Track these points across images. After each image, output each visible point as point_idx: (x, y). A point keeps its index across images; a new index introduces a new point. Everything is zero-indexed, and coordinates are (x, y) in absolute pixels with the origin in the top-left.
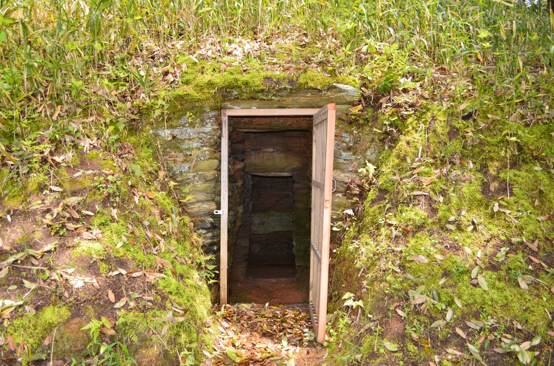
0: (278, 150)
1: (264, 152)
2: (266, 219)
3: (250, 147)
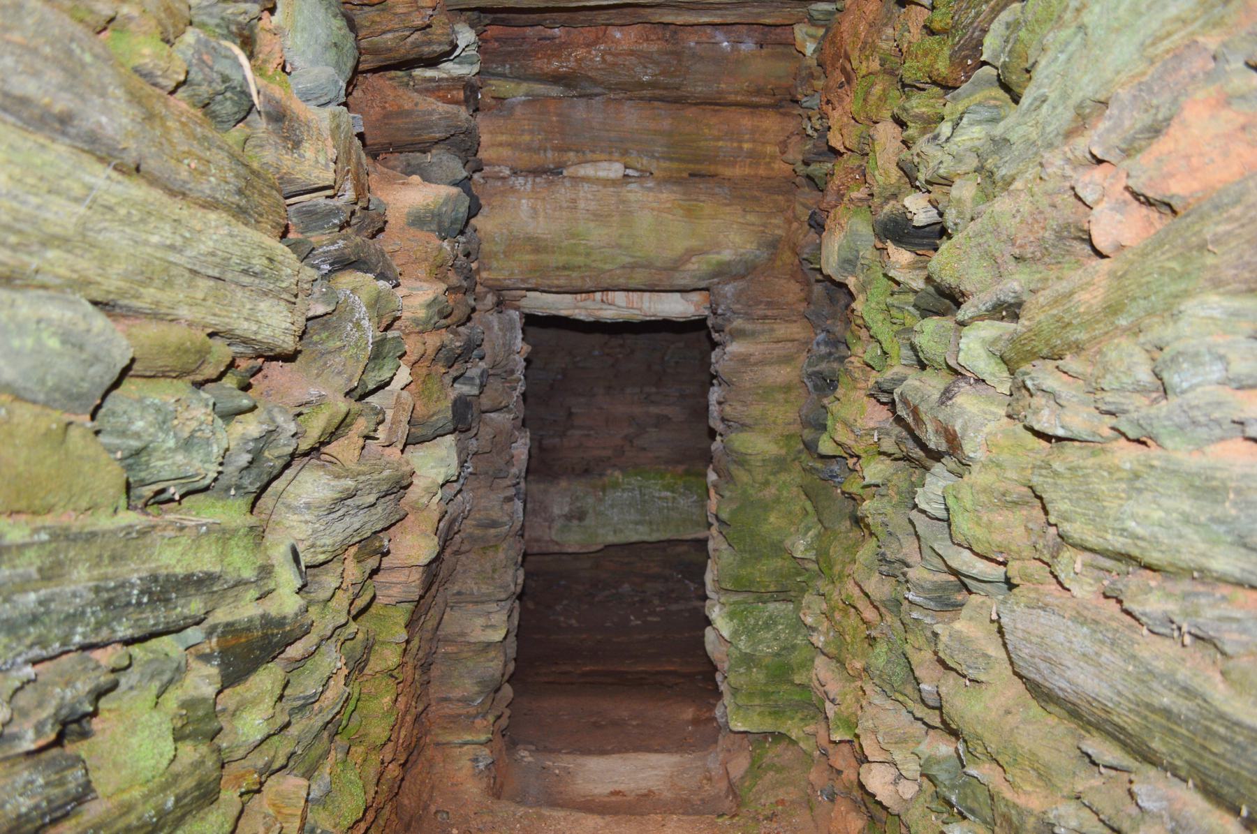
0: (645, 174)
1: (576, 180)
2: (591, 500)
3: (506, 152)
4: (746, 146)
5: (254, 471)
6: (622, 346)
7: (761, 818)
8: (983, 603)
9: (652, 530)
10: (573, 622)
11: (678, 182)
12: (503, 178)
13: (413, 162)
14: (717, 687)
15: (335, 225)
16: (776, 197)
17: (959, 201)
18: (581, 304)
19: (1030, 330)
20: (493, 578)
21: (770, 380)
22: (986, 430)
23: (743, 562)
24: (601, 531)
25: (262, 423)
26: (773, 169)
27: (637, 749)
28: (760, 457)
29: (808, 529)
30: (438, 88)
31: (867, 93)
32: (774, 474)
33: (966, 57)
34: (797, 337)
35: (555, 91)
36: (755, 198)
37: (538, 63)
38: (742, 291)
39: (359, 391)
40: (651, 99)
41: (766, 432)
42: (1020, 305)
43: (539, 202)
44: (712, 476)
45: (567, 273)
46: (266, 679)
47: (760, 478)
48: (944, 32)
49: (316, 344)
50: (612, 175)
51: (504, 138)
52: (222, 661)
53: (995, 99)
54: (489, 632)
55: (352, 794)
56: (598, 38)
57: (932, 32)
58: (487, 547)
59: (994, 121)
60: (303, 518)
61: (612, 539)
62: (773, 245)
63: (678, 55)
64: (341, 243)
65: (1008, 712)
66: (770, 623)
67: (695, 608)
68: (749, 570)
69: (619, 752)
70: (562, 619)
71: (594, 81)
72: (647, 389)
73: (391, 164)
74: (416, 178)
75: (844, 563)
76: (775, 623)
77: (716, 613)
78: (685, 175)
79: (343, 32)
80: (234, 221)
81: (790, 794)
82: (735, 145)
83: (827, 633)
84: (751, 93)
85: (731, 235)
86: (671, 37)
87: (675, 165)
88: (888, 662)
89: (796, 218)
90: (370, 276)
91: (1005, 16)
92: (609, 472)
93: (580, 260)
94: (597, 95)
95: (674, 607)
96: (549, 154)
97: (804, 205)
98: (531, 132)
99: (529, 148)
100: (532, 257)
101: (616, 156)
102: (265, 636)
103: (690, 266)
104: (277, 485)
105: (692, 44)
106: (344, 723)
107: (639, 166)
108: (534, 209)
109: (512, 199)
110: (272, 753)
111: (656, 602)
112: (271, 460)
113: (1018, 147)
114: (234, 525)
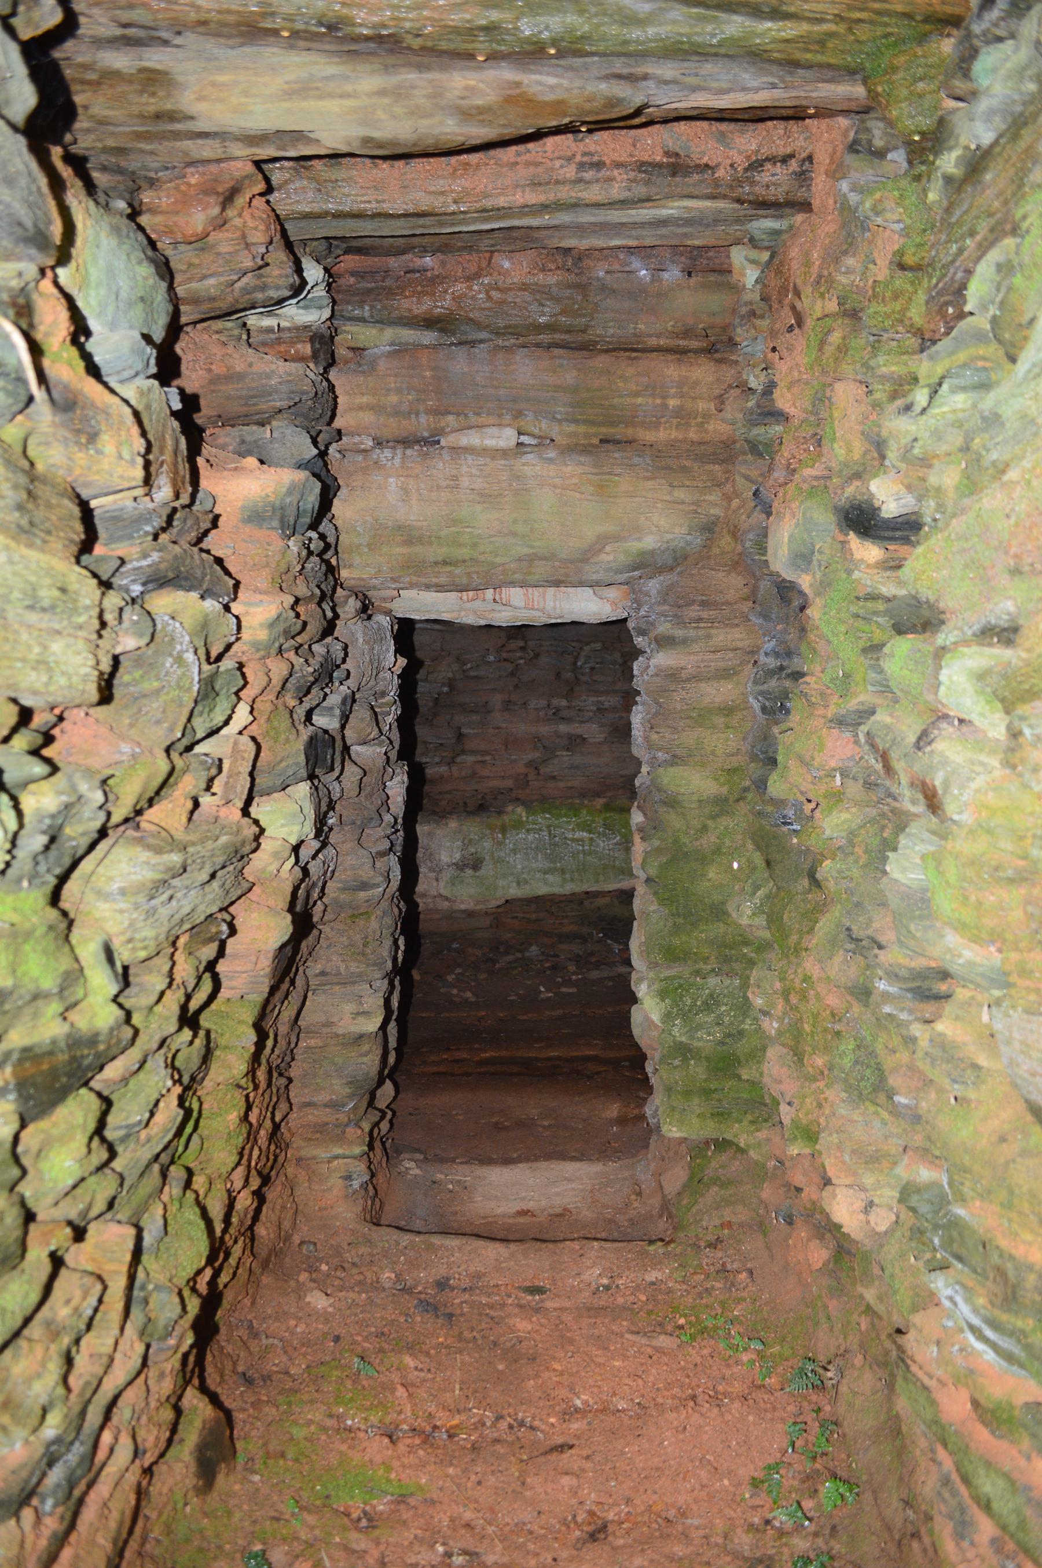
0: (545, 441)
2: (487, 844)
4: (672, 403)
5: (53, 853)
6: (523, 649)
7: (703, 1244)
8: (972, 998)
9: (565, 881)
10: (468, 994)
11: (586, 450)
12: (365, 451)
13: (248, 439)
14: (647, 1079)
15: (147, 533)
16: (710, 467)
17: (938, 490)
18: (468, 605)
19: (1028, 665)
20: (364, 954)
21: (707, 700)
22: (973, 785)
23: (676, 929)
24: (501, 883)
25: (62, 793)
26: (706, 431)
27: (548, 1157)
28: (695, 798)
29: (757, 888)
30: (279, 341)
31: (823, 343)
32: (713, 817)
33: (947, 304)
34: (740, 644)
35: (429, 337)
36: (684, 470)
37: (405, 303)
38: (670, 587)
39: (185, 742)
40: (549, 346)
41: (703, 765)
42: (1015, 630)
43: (411, 481)
44: (637, 818)
45: (448, 569)
46: (77, 1111)
47: (696, 823)
48: (917, 268)
49: (128, 685)
50: (502, 444)
51: (365, 400)
52: (20, 1095)
53: (984, 358)
54: (361, 1019)
55: (191, 1239)
56: (480, 269)
57: (902, 267)
58: (357, 915)
59: (984, 386)
60: (116, 906)
61: (514, 892)
62: (709, 528)
63: (583, 288)
64: (155, 556)
65: (1003, 1139)
66: (711, 1003)
67: (620, 975)
68: (684, 938)
69: (527, 1160)
70: (455, 991)
71: (477, 325)
72: (555, 702)
73: (221, 441)
74: (251, 461)
75: (801, 933)
76: (718, 1004)
77: (642, 990)
78: (595, 441)
79: (151, 281)
80: (13, 544)
81: (740, 1215)
82: (658, 401)
83: (781, 1020)
84: (677, 335)
85: (656, 517)
86: (575, 264)
87: (582, 429)
88: (856, 1062)
89: (737, 494)
90: (194, 595)
91: (994, 256)
92: (510, 808)
93: (464, 553)
94: (481, 341)
95: (595, 974)
96: (423, 419)
97: (747, 478)
98: (399, 391)
99: (397, 413)
100: (404, 550)
101: (508, 418)
102: (73, 1059)
103: (603, 557)
104: (86, 866)
105: (601, 274)
106: (181, 1149)
107: (536, 431)
108: (405, 490)
109: (377, 478)
110: (88, 1199)
111: (572, 968)
112: (73, 839)
113: (1012, 426)
114: (27, 925)
